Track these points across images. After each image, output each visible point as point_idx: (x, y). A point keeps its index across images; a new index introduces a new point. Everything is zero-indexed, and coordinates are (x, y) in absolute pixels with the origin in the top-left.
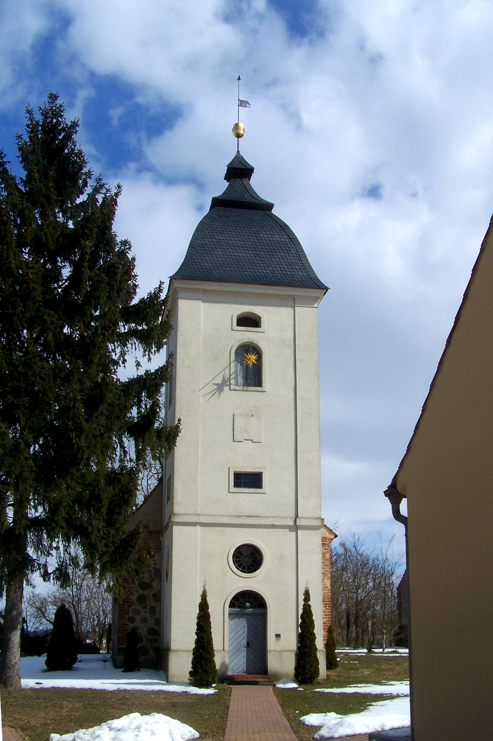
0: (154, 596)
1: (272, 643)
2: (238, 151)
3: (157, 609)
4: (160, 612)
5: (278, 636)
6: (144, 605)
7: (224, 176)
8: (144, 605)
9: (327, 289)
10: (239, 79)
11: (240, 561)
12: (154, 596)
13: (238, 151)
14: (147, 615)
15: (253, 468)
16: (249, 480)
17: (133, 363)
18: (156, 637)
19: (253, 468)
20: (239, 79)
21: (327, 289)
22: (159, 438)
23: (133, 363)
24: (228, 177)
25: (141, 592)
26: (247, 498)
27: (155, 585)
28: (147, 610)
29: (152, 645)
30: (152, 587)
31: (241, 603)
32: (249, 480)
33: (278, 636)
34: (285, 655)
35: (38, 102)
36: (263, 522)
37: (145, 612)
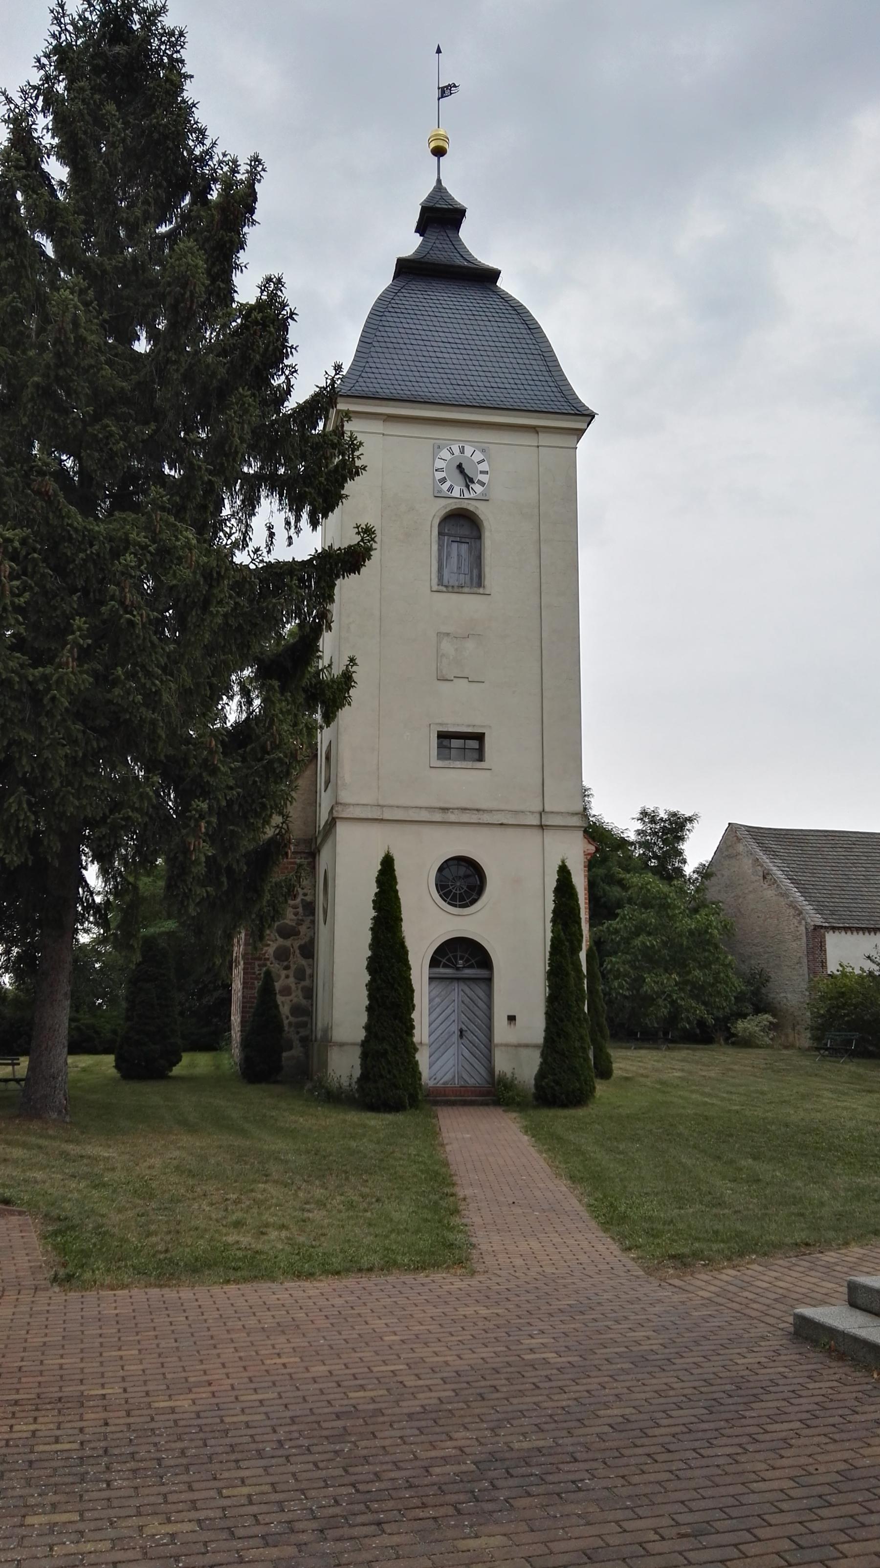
0: (301, 948)
1: (502, 1032)
2: (439, 181)
3: (308, 972)
4: (312, 976)
5: (512, 1019)
6: (285, 963)
7: (415, 225)
8: (285, 963)
9: (592, 416)
10: (439, 51)
11: (451, 891)
12: (301, 948)
13: (439, 181)
14: (291, 980)
15: (469, 726)
16: (462, 744)
17: (273, 534)
18: (305, 1019)
19: (469, 726)
20: (439, 51)
21: (592, 416)
22: (308, 689)
23: (273, 534)
24: (421, 229)
25: (281, 941)
26: (460, 783)
27: (303, 929)
28: (291, 973)
29: (298, 1033)
30: (298, 933)
31: (449, 960)
32: (462, 744)
33: (512, 1019)
34: (524, 1052)
35: (580, 834)
36: (486, 818)
37: (287, 977)
